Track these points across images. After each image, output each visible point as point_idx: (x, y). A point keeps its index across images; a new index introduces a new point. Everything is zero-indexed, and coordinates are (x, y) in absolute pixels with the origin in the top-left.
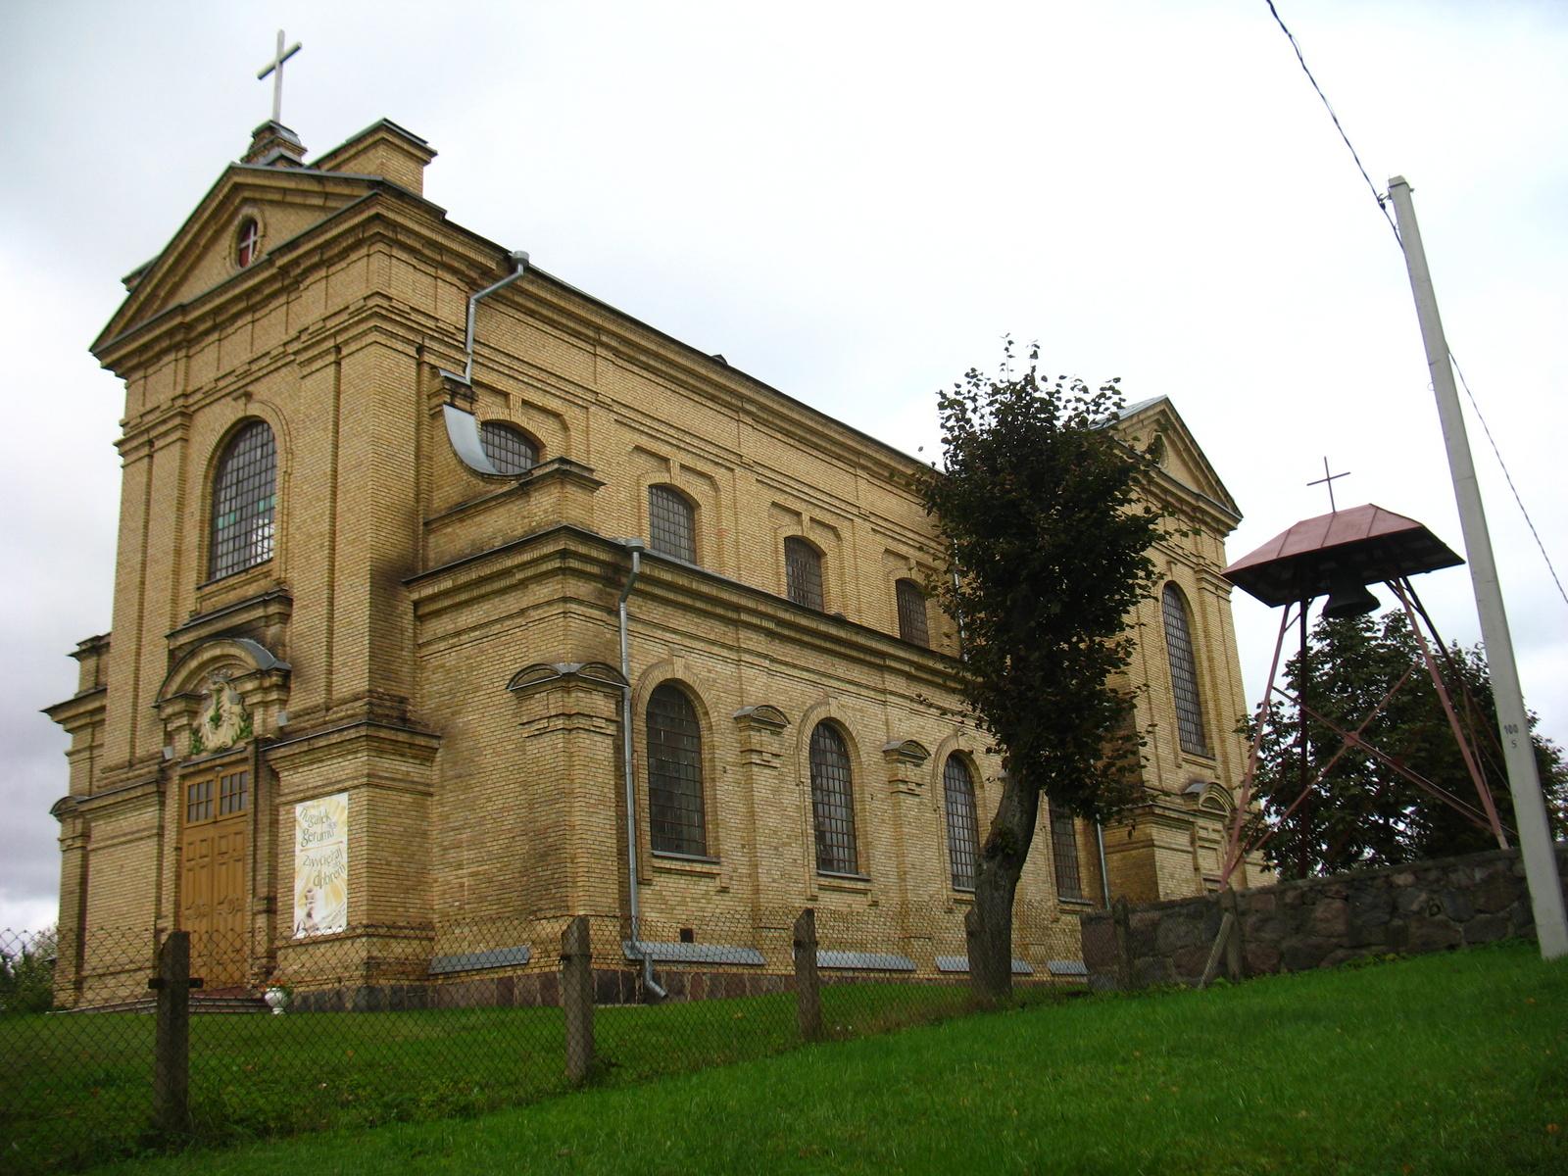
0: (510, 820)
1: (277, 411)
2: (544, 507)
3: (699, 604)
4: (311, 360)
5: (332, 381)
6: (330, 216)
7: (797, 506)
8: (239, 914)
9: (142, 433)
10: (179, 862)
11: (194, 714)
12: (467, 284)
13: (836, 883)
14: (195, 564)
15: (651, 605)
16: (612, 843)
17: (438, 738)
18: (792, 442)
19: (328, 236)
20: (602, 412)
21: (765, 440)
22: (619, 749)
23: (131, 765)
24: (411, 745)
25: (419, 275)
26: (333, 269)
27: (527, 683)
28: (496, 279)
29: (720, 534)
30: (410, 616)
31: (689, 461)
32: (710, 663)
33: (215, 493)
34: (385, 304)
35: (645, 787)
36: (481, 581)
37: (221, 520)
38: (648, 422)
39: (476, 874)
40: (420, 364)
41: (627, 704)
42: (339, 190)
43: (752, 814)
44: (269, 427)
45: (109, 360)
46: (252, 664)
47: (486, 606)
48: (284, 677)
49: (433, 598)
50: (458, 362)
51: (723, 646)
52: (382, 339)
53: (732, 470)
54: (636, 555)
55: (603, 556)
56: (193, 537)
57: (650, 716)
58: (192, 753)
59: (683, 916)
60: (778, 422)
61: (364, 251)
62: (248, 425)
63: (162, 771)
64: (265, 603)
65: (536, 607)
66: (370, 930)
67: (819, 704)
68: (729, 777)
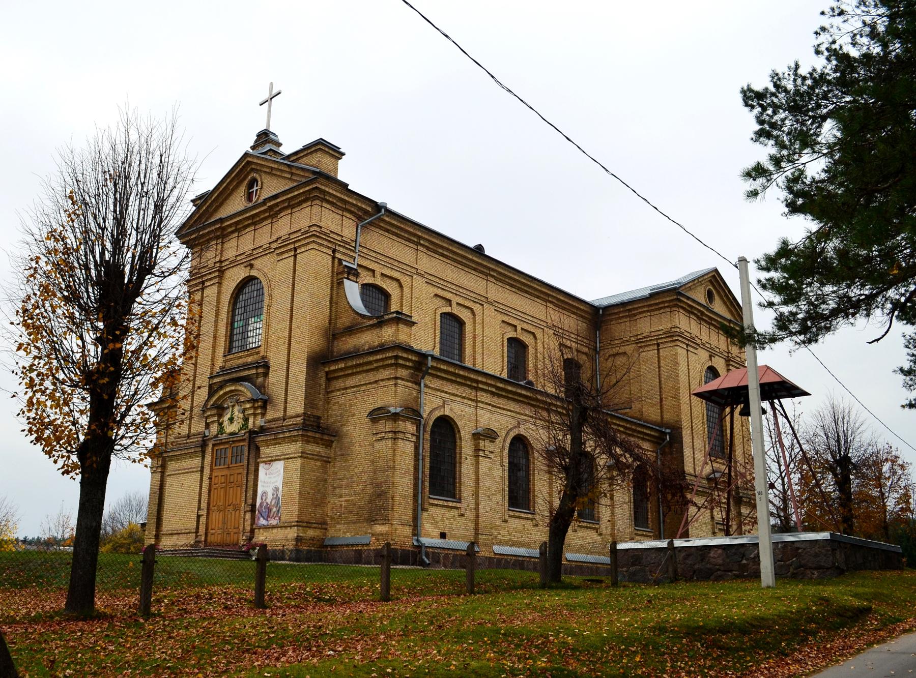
0: (365, 477)
1: (265, 275)
2: (388, 334)
3: (458, 380)
4: (282, 253)
5: (292, 264)
6: (295, 184)
7: (515, 322)
8: (238, 512)
9: (199, 278)
10: (210, 484)
11: (220, 416)
12: (357, 218)
13: (517, 514)
14: (223, 344)
15: (436, 380)
16: (411, 492)
17: (334, 436)
18: (514, 290)
19: (293, 194)
20: (419, 278)
21: (500, 289)
22: (417, 448)
23: (189, 436)
24: (322, 439)
25: (335, 214)
26: (294, 210)
27: (377, 415)
28: (371, 215)
29: (474, 337)
30: (324, 379)
31: (461, 301)
32: (463, 407)
33: (234, 310)
34: (318, 230)
35: (428, 465)
36: (358, 365)
37: (236, 323)
38: (442, 282)
39: (348, 500)
40: (334, 258)
41: (422, 427)
42: (298, 172)
43: (477, 480)
44: (261, 282)
45: (184, 240)
46: (249, 395)
47: (360, 377)
48: (264, 403)
49: (335, 371)
50: (351, 257)
51: (469, 399)
52: (316, 246)
53: (483, 305)
54: (430, 358)
55: (414, 358)
56: (222, 331)
57: (432, 432)
58: (218, 434)
59: (442, 528)
60: (507, 280)
61: (309, 203)
62: (249, 281)
63: (204, 441)
64: (257, 368)
65: (382, 380)
66: (299, 524)
67: (515, 427)
68: (468, 461)
